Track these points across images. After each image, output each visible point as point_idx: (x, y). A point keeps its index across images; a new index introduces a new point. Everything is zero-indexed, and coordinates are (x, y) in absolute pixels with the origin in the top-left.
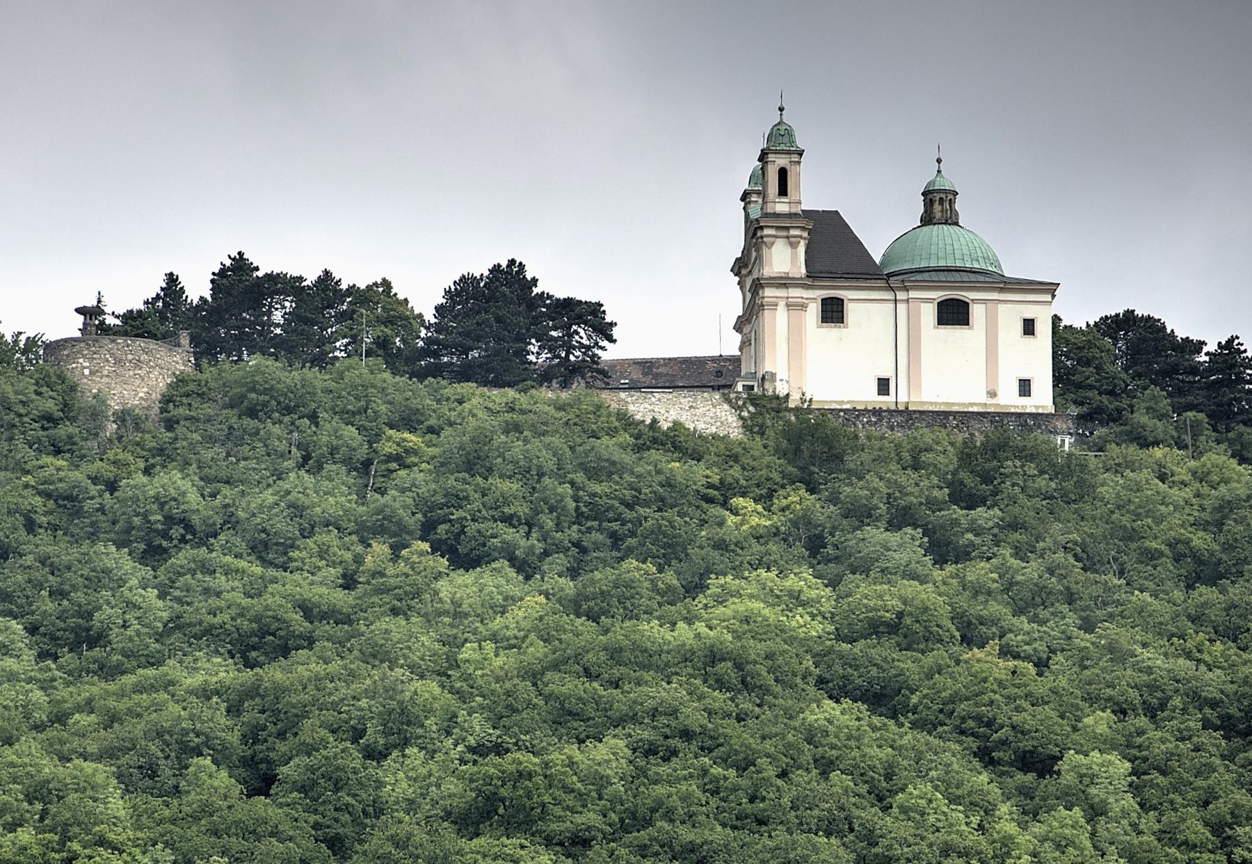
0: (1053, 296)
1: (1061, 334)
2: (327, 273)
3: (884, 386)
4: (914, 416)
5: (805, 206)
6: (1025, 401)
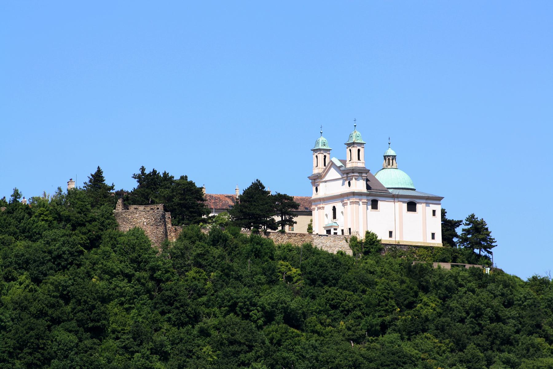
3: (314, 231)
6: (433, 241)
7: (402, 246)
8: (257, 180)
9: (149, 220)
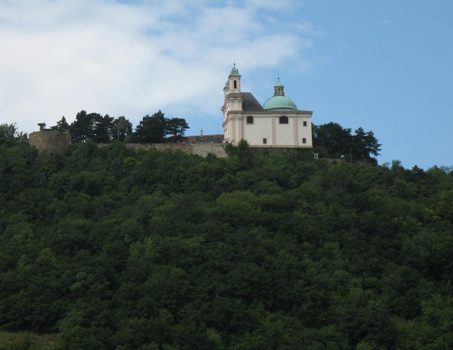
0: (311, 115)
1: (314, 128)
2: (371, 131)
3: (265, 141)
4: (274, 149)
5: (242, 91)
7: (274, 149)
8: (160, 111)
9: (44, 138)
